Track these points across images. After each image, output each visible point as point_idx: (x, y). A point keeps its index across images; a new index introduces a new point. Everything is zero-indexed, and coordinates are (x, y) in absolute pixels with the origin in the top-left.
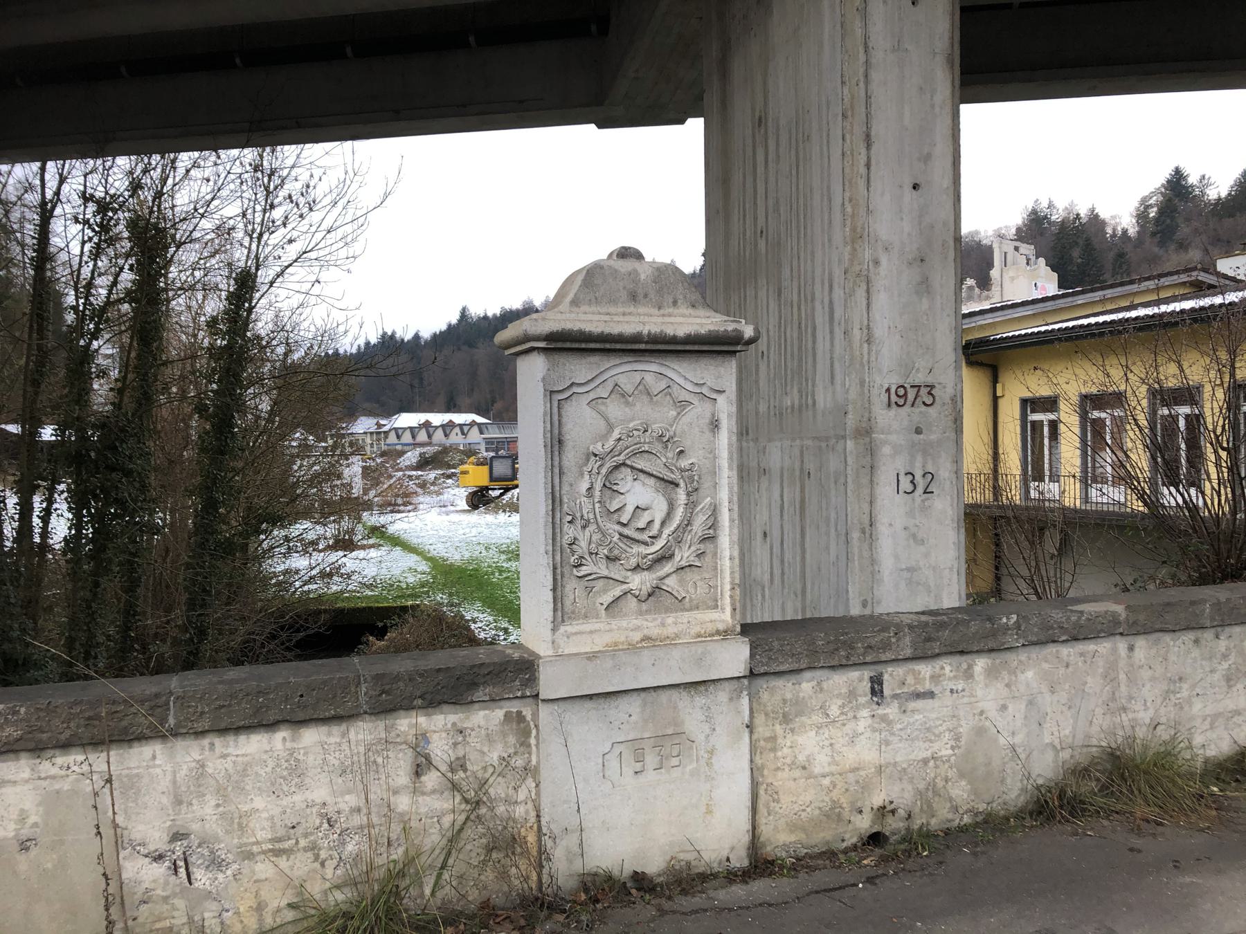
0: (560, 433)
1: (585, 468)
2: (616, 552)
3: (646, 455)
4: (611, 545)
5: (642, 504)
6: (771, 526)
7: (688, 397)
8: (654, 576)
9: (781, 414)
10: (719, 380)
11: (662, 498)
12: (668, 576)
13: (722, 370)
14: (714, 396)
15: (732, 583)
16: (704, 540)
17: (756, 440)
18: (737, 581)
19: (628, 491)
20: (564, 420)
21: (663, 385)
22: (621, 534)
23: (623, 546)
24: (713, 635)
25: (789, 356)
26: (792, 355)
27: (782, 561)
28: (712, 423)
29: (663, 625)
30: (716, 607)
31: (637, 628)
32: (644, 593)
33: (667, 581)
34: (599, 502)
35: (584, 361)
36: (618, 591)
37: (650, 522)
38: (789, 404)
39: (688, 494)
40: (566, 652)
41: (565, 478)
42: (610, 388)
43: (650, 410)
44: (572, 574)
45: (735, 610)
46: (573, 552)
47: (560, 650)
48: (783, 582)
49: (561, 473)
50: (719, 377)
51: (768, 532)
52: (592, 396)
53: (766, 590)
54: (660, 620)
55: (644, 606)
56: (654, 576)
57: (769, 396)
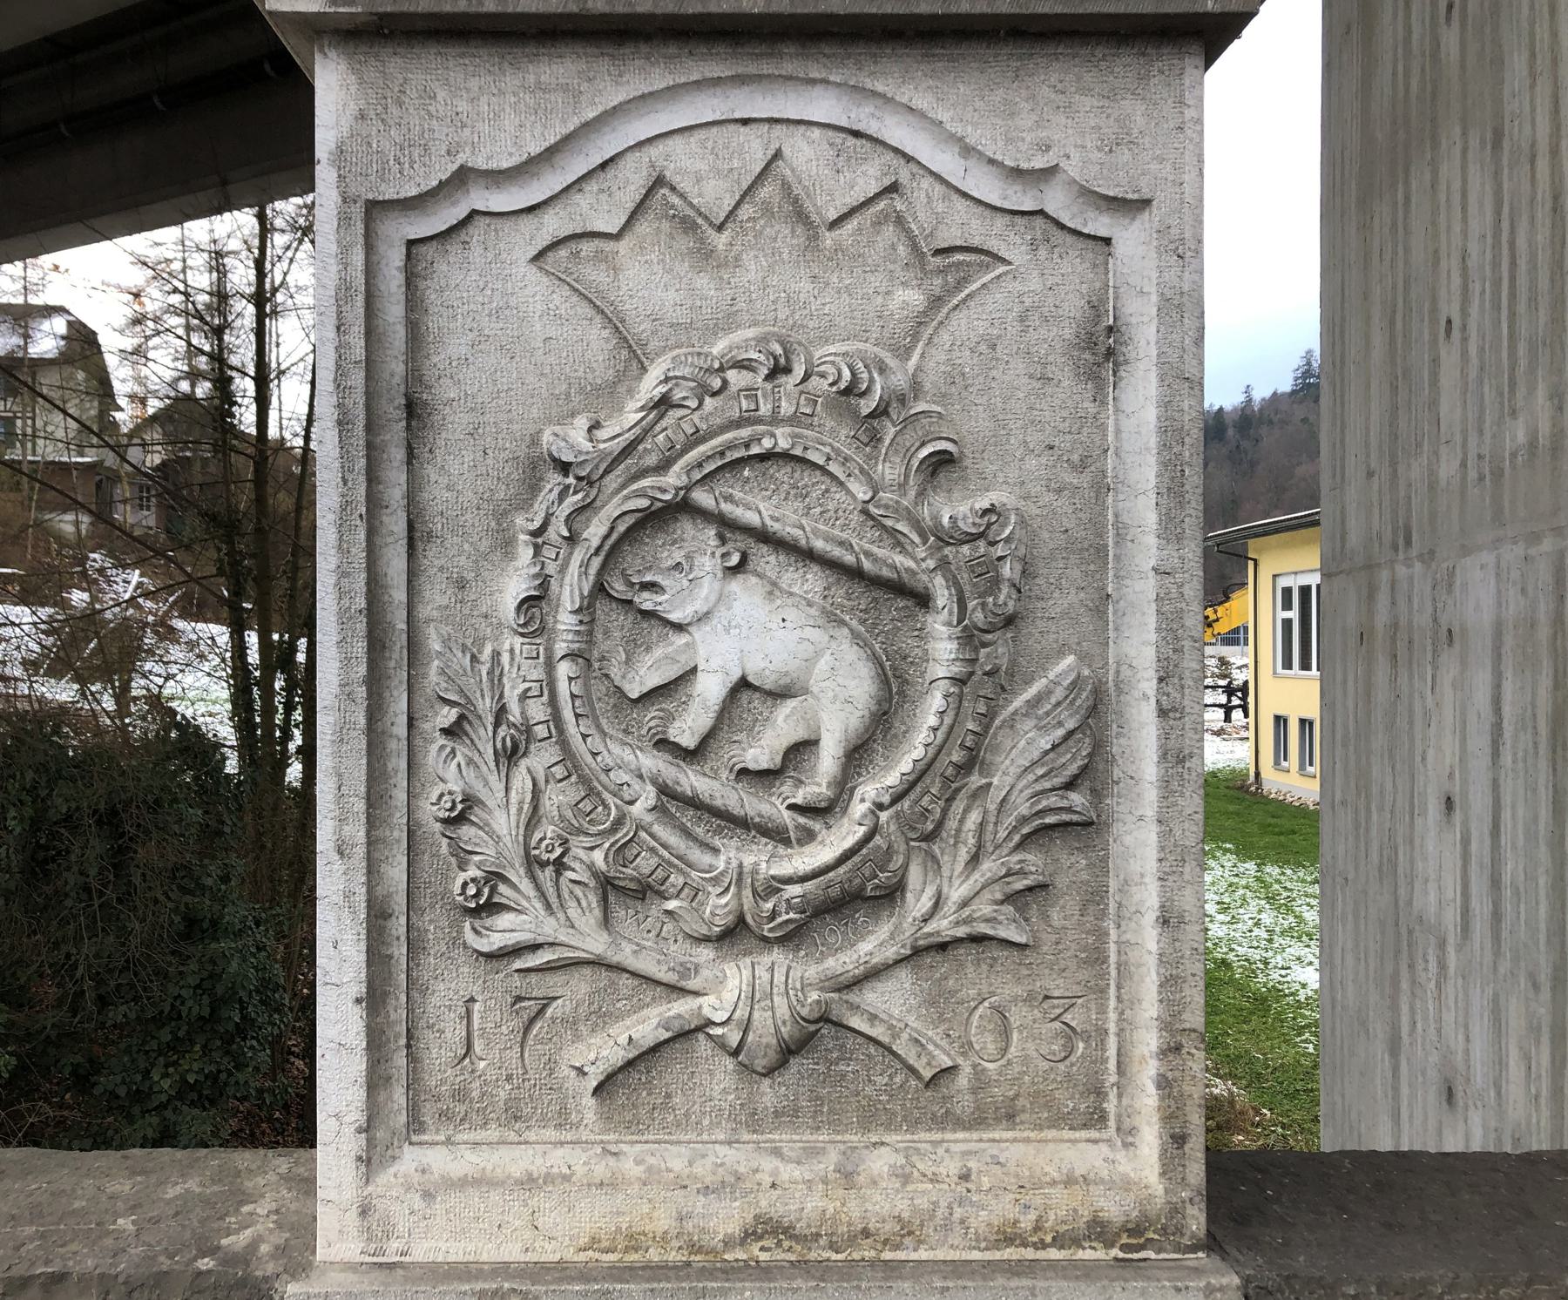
0: (415, 375)
1: (520, 521)
2: (645, 863)
3: (782, 473)
4: (622, 835)
5: (765, 665)
6: (1464, 781)
7: (979, 230)
8: (813, 972)
9: (1498, 474)
10: (1124, 155)
11: (850, 653)
12: (874, 974)
13: (1135, 112)
14: (1099, 224)
15: (1168, 1025)
16: (1040, 834)
17: (1429, 557)
18: (1195, 1018)
19: (703, 618)
20: (434, 323)
21: (867, 180)
22: (665, 791)
23: (673, 839)
24: (1076, 1242)
25: (1522, 307)
26: (1533, 300)
27: (1496, 883)
28: (1090, 343)
29: (847, 1176)
30: (1096, 1118)
31: (728, 1185)
32: (765, 1033)
33: (873, 997)
34: (570, 656)
35: (511, 80)
36: (646, 1026)
37: (801, 750)
38: (1521, 437)
39: (970, 638)
40: (422, 1252)
41: (432, 558)
42: (630, 195)
43: (806, 285)
44: (457, 941)
45: (1179, 1140)
46: (462, 856)
47: (395, 1245)
48: (1496, 938)
49: (414, 539)
50: (1121, 140)
51: (1457, 799)
52: (553, 224)
53: (1451, 949)
54: (833, 1157)
55: (769, 1094)
56: (813, 972)
57: (1464, 432)
